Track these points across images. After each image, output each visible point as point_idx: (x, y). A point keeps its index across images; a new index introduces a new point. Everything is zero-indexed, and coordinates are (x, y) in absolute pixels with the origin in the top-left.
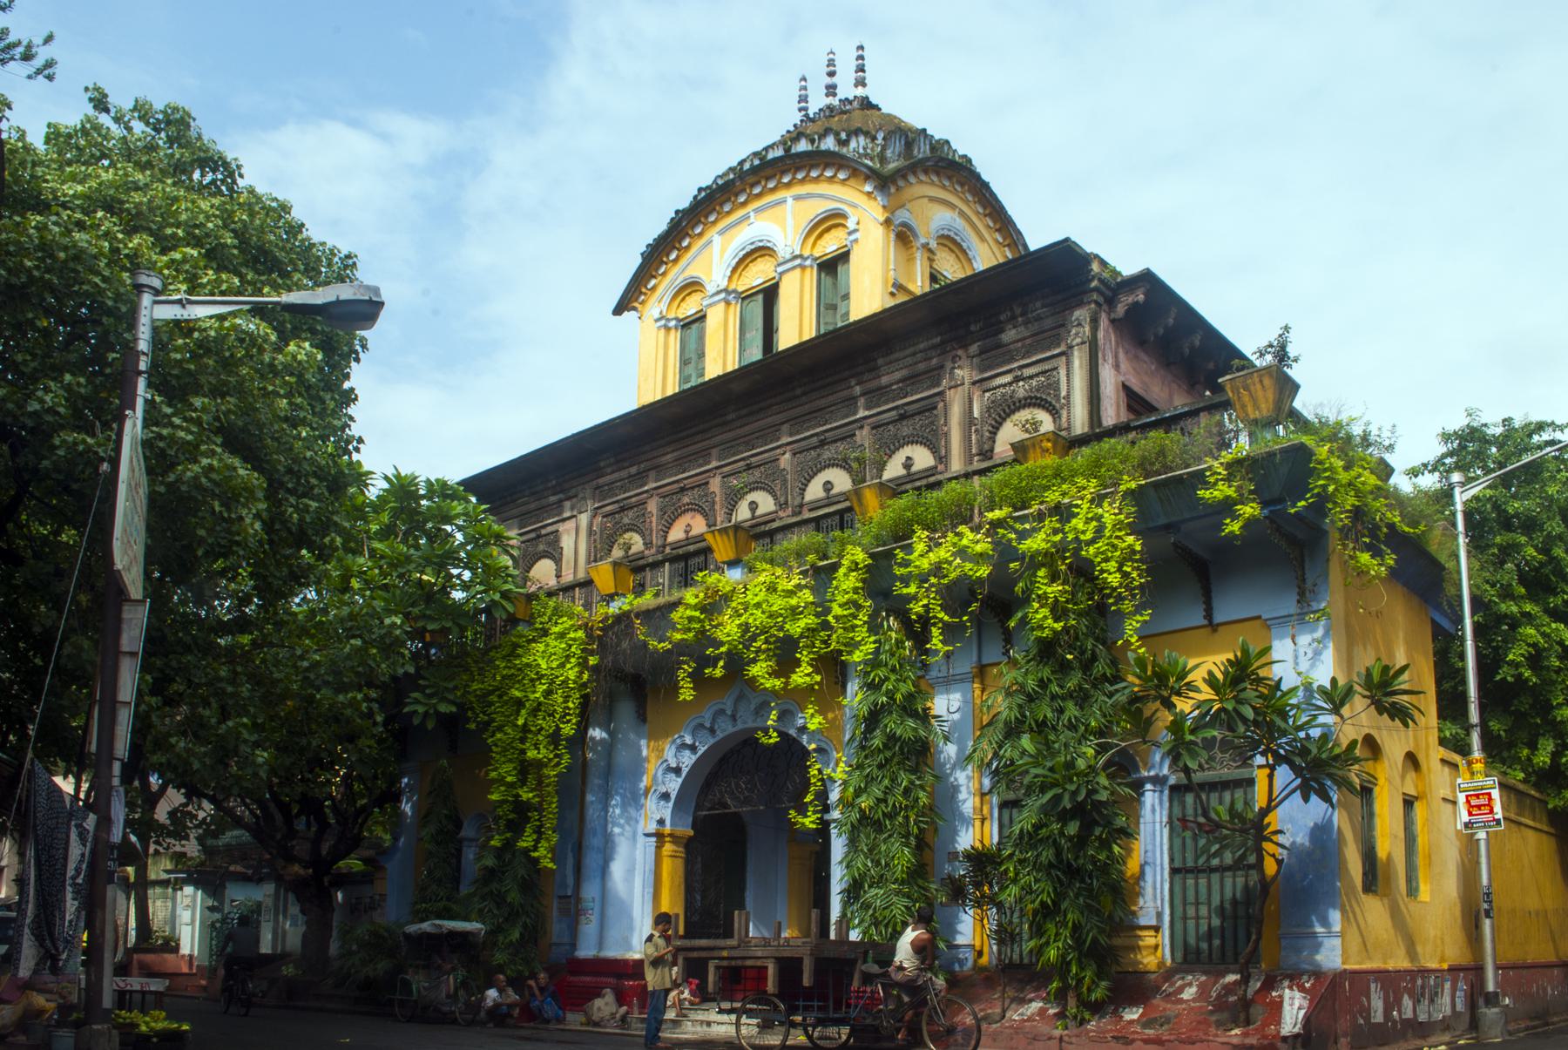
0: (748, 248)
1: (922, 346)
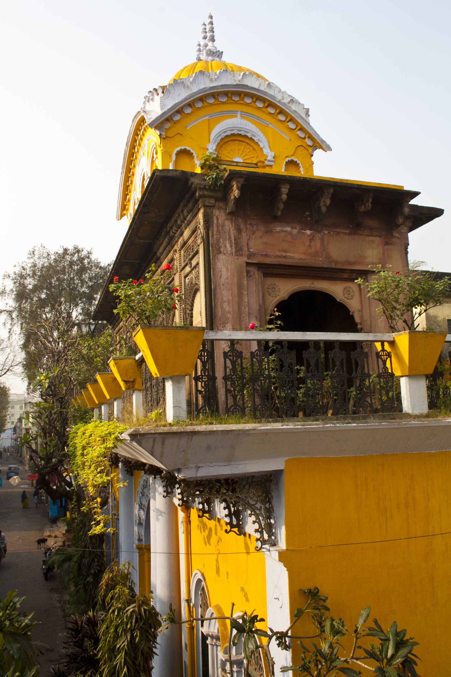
0: (229, 133)
1: (164, 244)
